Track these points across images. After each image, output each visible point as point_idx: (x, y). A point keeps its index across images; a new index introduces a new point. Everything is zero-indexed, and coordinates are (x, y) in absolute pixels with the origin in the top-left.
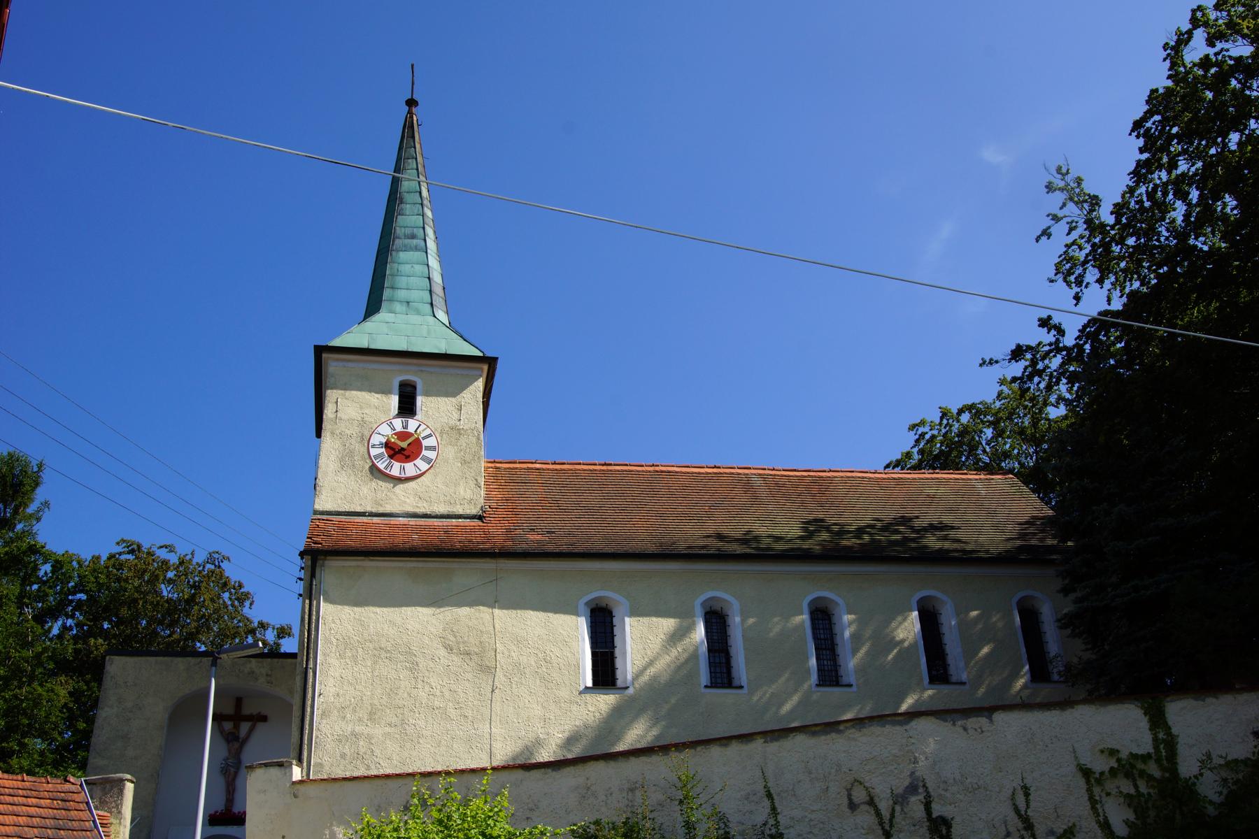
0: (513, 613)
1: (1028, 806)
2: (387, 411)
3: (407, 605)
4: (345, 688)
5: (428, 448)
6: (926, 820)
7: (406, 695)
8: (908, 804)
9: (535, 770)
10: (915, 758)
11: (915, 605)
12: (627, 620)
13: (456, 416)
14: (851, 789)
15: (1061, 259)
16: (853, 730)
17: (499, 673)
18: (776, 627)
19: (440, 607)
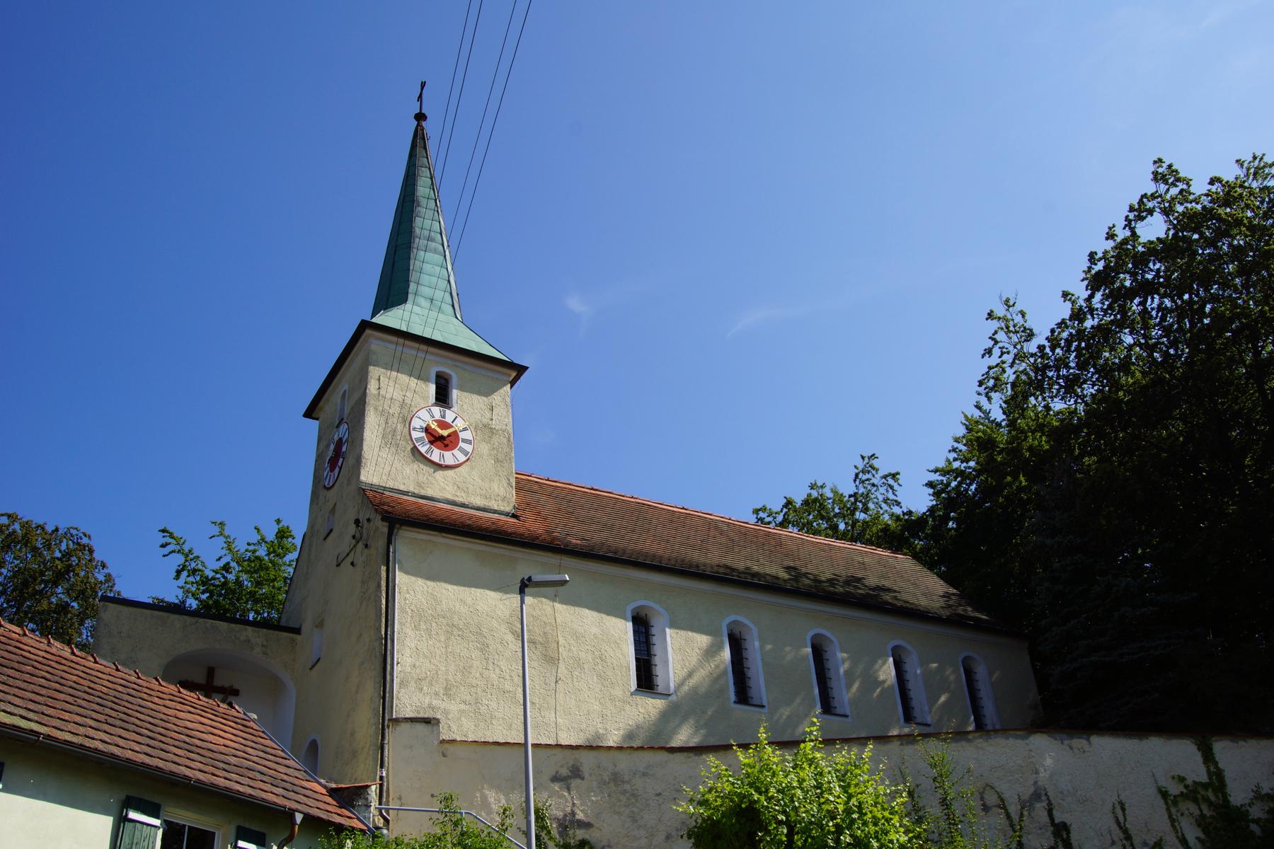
0: (572, 609)
1: (1125, 820)
2: (425, 398)
3: (476, 587)
4: (421, 660)
5: (465, 441)
6: (1049, 825)
7: (478, 675)
8: (1034, 810)
9: (678, 754)
10: (1036, 769)
11: (890, 653)
12: (668, 630)
13: (488, 415)
14: (983, 792)
15: (984, 377)
16: (981, 740)
17: (562, 666)
18: (789, 654)
19: (506, 593)
